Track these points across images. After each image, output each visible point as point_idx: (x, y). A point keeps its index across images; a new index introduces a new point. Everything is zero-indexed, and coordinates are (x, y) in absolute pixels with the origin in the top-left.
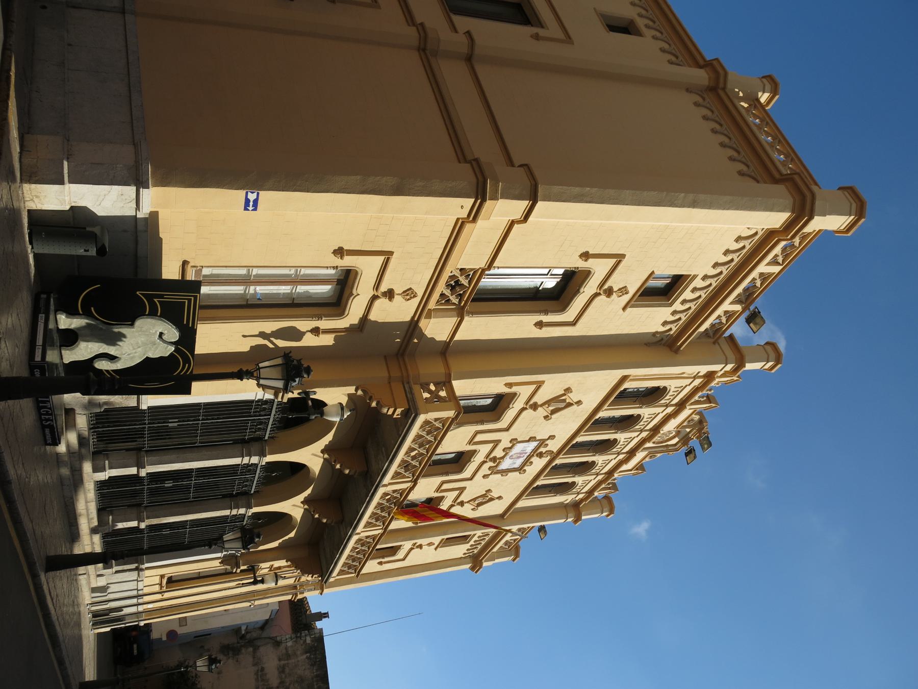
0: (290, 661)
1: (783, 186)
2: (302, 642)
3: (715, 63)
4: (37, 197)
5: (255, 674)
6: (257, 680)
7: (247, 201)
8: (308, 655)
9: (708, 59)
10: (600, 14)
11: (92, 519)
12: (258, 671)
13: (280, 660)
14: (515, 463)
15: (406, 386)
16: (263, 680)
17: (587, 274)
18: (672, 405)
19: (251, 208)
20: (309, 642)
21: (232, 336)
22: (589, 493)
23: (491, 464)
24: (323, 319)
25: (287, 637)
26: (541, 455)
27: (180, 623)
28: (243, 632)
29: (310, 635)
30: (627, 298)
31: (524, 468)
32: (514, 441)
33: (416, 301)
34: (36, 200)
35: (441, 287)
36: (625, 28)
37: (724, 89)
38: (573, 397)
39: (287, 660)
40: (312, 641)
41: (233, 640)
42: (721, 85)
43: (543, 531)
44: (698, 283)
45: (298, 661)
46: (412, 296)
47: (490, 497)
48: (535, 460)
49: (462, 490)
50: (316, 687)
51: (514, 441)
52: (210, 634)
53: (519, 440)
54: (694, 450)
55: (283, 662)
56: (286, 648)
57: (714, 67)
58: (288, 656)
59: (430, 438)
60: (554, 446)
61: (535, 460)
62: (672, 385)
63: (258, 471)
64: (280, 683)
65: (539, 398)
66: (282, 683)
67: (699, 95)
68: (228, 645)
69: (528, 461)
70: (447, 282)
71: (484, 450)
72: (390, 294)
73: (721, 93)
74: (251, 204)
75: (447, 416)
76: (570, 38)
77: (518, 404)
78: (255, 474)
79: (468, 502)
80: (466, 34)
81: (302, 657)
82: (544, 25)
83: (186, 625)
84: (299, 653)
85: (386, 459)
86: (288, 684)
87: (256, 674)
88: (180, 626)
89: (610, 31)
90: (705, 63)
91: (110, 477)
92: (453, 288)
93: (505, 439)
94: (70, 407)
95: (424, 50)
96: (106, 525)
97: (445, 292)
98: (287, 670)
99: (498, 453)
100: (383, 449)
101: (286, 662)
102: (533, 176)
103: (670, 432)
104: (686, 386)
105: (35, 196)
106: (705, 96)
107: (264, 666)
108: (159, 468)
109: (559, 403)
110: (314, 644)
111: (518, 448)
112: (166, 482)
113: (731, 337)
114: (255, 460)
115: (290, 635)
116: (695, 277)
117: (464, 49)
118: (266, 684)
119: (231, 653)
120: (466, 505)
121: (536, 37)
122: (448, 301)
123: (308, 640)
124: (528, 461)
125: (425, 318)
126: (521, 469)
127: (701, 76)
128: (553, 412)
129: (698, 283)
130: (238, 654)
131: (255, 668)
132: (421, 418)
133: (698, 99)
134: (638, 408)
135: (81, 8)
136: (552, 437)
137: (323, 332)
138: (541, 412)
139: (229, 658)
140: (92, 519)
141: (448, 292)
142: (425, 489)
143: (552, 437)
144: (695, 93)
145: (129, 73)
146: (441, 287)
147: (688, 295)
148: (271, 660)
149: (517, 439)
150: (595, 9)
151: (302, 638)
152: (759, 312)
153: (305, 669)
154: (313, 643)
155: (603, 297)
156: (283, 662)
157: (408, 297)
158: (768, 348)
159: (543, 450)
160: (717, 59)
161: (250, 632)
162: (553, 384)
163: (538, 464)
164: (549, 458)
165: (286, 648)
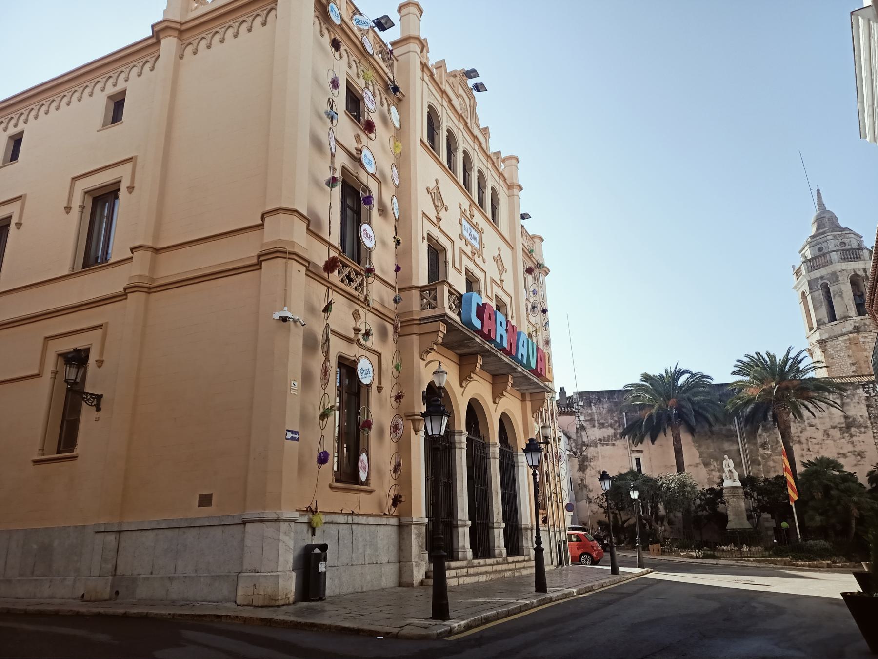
0: (596, 419)
2: (582, 409)
3: (156, 29)
4: (286, 595)
5: (603, 446)
6: (607, 445)
7: (292, 439)
8: (592, 404)
9: (151, 34)
10: (102, 127)
11: (497, 561)
12: (600, 444)
13: (594, 426)
16: (608, 440)
18: (442, 101)
19: (297, 436)
20: (583, 403)
21: (254, 459)
28: (572, 453)
29: (578, 402)
31: (480, 229)
32: (461, 237)
34: (289, 596)
36: (117, 105)
37: (181, 24)
38: (432, 185)
39: (595, 420)
40: (582, 401)
41: (576, 461)
42: (178, 26)
43: (525, 216)
45: (596, 412)
46: (357, 313)
47: (498, 258)
48: (474, 221)
49: (493, 281)
50: (616, 400)
51: (461, 237)
53: (461, 233)
54: (476, 84)
55: (596, 424)
56: (586, 421)
57: (159, 31)
58: (592, 420)
60: (466, 204)
61: (474, 221)
64: (612, 427)
65: (432, 215)
66: (611, 426)
67: (186, 47)
68: (579, 465)
69: (475, 226)
71: (467, 262)
73: (184, 27)
74: (294, 436)
75: (448, 293)
76: (131, 158)
77: (436, 233)
78: (472, 439)
79: (501, 275)
80: (133, 251)
81: (594, 410)
82: (118, 179)
84: (590, 411)
85: (474, 341)
86: (613, 421)
87: (603, 445)
89: (121, 120)
90: (155, 36)
91: (470, 548)
92: (351, 280)
93: (459, 244)
94: (424, 575)
95: (150, 288)
97: (354, 287)
98: (602, 421)
99: (468, 250)
100: (466, 342)
101: (596, 422)
102: (271, 212)
103: (460, 103)
104: (428, 88)
105: (286, 596)
106: (187, 42)
107: (597, 439)
109: (436, 197)
113: (392, 44)
114: (464, 439)
116: (348, 74)
117: (148, 254)
118: (611, 438)
119: (586, 464)
120: (503, 278)
121: (131, 189)
122: (361, 284)
123: (581, 403)
124: (475, 226)
127: (169, 44)
130: (587, 458)
131: (599, 445)
132: (448, 311)
133: (190, 49)
134: (442, 130)
135: (116, 564)
136: (460, 206)
137: (380, 384)
138: (442, 214)
139: (589, 465)
141: (354, 285)
143: (460, 206)
144: (184, 51)
145: (177, 528)
146: (350, 289)
147: (361, 83)
148: (594, 433)
149: (460, 234)
150: (98, 131)
152: (377, 19)
153: (603, 408)
156: (596, 424)
160: (153, 26)
161: (571, 448)
162: (423, 203)
163: (478, 218)
165: (586, 421)
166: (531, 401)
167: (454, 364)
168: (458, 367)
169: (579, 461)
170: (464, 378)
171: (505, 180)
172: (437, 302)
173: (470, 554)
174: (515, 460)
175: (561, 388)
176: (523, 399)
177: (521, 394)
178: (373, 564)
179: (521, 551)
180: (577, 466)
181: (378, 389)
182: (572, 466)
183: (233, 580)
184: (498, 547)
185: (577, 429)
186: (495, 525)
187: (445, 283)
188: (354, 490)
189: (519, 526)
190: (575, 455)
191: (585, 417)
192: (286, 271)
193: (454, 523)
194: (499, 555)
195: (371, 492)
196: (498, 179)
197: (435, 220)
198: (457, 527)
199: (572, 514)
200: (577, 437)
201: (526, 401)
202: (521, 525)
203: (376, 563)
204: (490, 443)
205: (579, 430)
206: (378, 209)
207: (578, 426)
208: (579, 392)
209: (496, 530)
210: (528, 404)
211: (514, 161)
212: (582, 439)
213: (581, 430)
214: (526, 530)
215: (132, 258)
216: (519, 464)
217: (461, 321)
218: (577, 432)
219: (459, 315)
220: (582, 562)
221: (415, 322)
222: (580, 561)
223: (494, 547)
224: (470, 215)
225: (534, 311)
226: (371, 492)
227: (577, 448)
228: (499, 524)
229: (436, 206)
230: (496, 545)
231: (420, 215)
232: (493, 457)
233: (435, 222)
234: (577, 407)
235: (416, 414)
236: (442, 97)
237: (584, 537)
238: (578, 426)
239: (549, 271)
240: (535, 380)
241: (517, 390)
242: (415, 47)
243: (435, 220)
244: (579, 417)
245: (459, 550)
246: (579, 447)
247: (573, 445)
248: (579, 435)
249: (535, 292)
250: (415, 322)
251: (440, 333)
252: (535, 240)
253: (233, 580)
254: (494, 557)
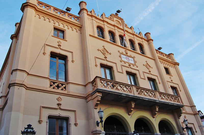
1: (25, 9)
14: (131, 60)
15: (93, 94)
22: (92, 16)
23: (132, 65)
26: (127, 53)
30: (171, 77)
33: (62, 97)
35: (59, 91)
37: (15, 34)
38: (145, 63)
42: (15, 35)
44: (165, 65)
48: (128, 55)
59: (174, 98)
60: (122, 50)
61: (128, 55)
62: (95, 25)
65: (148, 71)
69: (130, 57)
70: (65, 91)
72: (59, 105)
93: (119, 64)
111: (123, 59)
113: (79, 14)
120: (150, 70)
124: (130, 57)
126: (134, 58)
128: (150, 67)
129: (165, 65)
136: (119, 52)
138: (151, 70)
142: (146, 85)
157: (60, 99)
159: (124, 53)
164: (127, 51)
170: (153, 115)
197: (149, 72)
209: (66, 132)
215: (11, 74)
224: (126, 53)
229: (148, 68)
231: (166, 82)
233: (171, 82)
236: (114, 27)
242: (85, 12)
243: (149, 72)
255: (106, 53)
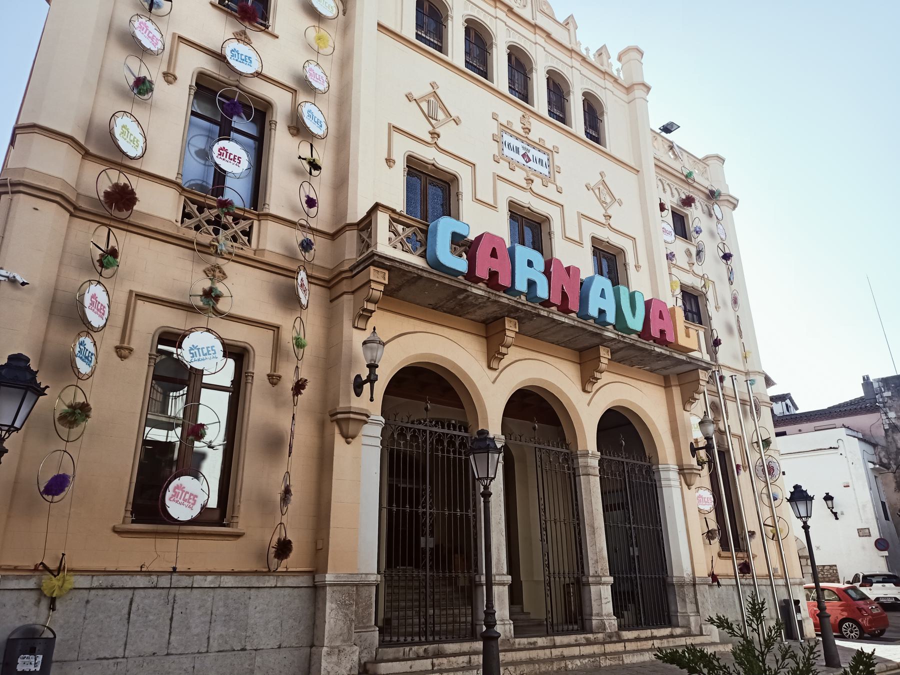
2: (889, 401)
17: (594, 239)
23: (537, 182)
24: (251, 370)
25: (885, 417)
27: (866, 536)
40: (889, 390)
48: (533, 136)
52: (883, 504)
61: (533, 136)
63: (620, 459)
68: (896, 482)
83: (869, 529)
88: (870, 536)
96: (604, 623)
108: (499, 560)
110: (893, 387)
112: (632, 554)
115: (882, 415)
123: (888, 394)
124: (539, 146)
125: (264, 257)
140: (587, 639)
151: (886, 401)
154: (891, 388)
155: (612, 222)
158: (624, 59)
159: (518, 128)
161: (880, 459)
166: (680, 385)
167: (475, 337)
168: (484, 341)
169: (895, 477)
171: (616, 80)
172: (184, 208)
173: (612, 623)
174: (656, 477)
175: (864, 378)
176: (667, 385)
177: (662, 377)
178: (234, 650)
179: (673, 620)
180: (894, 485)
181: (269, 379)
182: (885, 484)
183: (285, 666)
184: (598, 615)
185: (886, 431)
186: (591, 579)
187: (380, 208)
188: (183, 534)
189: (669, 580)
190: (888, 469)
191: (896, 413)
192: (9, 209)
193: (584, 579)
194: (598, 628)
195: (238, 536)
196: (603, 81)
198: (588, 584)
199: (887, 555)
200: (887, 442)
201: (671, 386)
202: (672, 577)
203: (243, 649)
204: (578, 453)
205: (890, 432)
206: (289, 127)
207: (887, 427)
208: (882, 379)
210: (676, 392)
211: (636, 55)
212: (897, 445)
213: (893, 432)
214: (682, 585)
216: (663, 483)
217: (429, 266)
218: (887, 436)
219: (423, 255)
220: (845, 633)
221: (344, 275)
222: (841, 631)
223: (591, 615)
225: (700, 257)
226: (238, 536)
227: (889, 459)
228: (598, 579)
230: (594, 612)
232: (584, 472)
234: (881, 400)
235: (338, 411)
237: (844, 593)
238: (887, 427)
239: (738, 201)
240: (658, 350)
241: (651, 371)
244: (886, 413)
245: (593, 618)
246: (893, 456)
247: (883, 454)
248: (890, 439)
249: (698, 229)
250: (344, 275)
251: (373, 285)
252: (709, 162)
253: (285, 666)
254: (592, 632)
255: (441, 115)
